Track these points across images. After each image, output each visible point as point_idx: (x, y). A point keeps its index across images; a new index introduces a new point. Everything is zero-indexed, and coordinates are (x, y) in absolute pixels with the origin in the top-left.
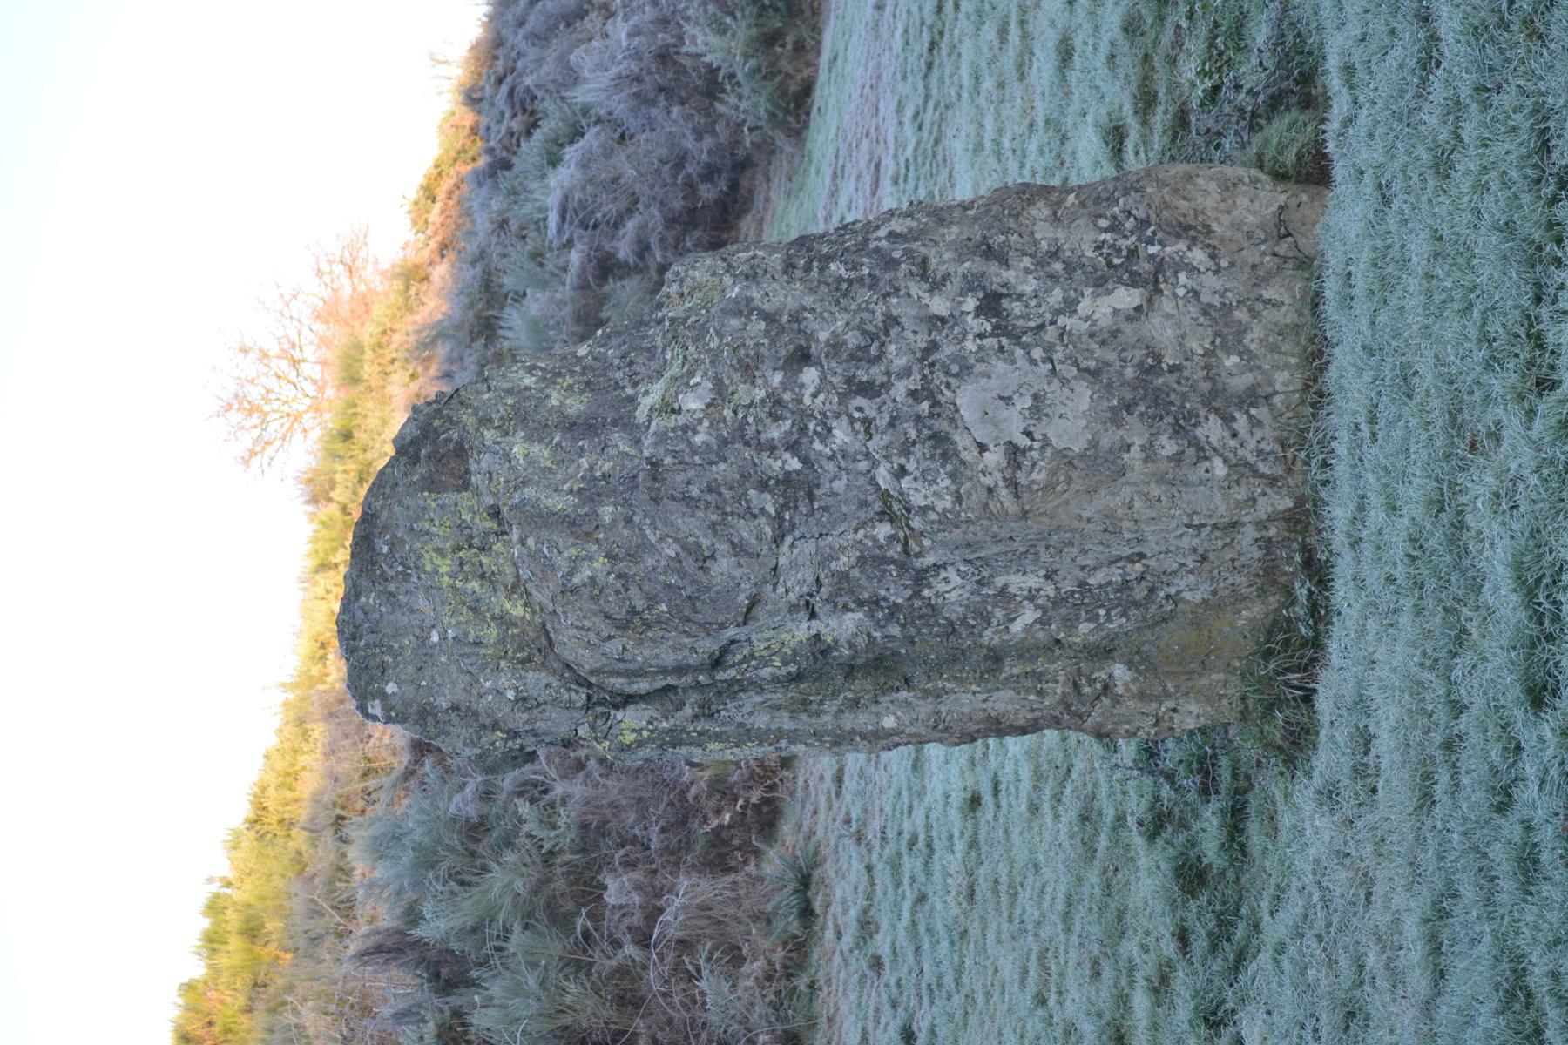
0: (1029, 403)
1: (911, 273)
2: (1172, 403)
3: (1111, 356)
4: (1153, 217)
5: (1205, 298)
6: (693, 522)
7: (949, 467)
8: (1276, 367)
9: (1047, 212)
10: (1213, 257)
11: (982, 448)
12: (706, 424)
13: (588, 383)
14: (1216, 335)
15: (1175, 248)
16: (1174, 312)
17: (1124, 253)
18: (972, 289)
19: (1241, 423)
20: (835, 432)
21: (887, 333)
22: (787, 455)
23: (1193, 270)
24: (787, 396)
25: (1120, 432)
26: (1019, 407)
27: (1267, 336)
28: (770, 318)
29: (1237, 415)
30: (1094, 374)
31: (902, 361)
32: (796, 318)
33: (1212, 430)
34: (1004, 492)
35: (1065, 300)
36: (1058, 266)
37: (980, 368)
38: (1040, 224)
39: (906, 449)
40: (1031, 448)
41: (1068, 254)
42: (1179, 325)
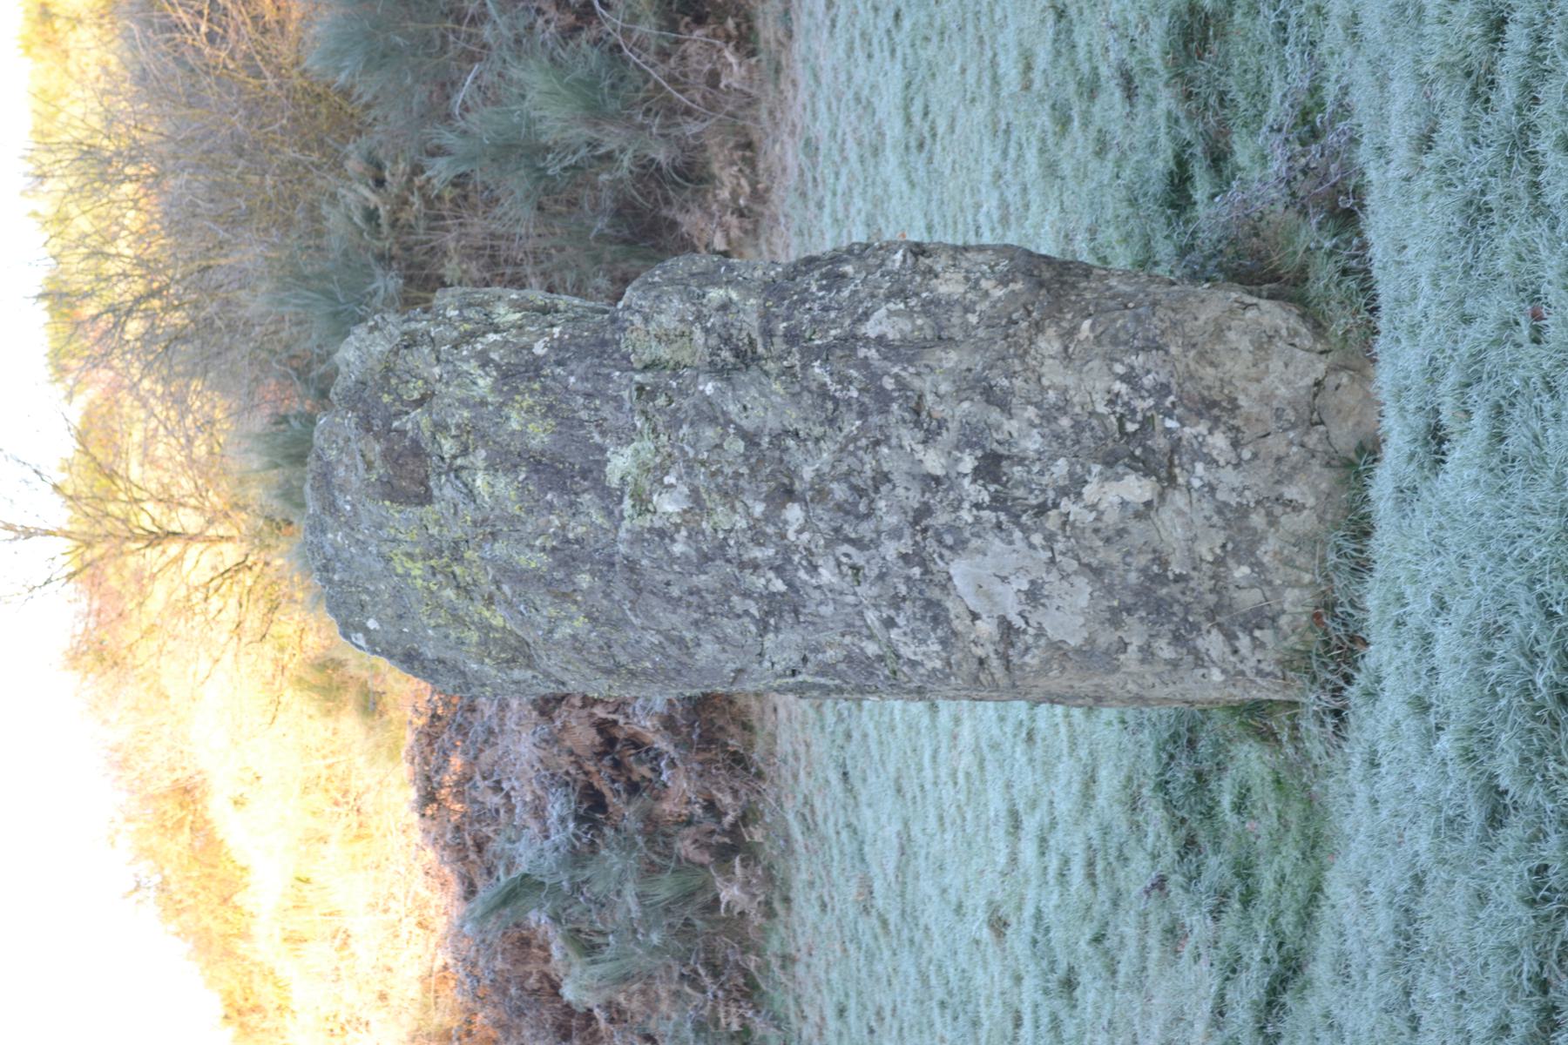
0: (1025, 587)
1: (904, 421)
2: (1174, 614)
3: (1115, 558)
4: (1174, 387)
5: (1221, 496)
6: (675, 619)
7: (940, 633)
8: (1289, 584)
9: (1057, 346)
10: (1236, 444)
11: (975, 616)
12: (684, 533)
13: (550, 407)
14: (1229, 538)
15: (1194, 431)
16: (1187, 509)
17: (1139, 417)
18: (971, 445)
19: (1244, 642)
20: (821, 570)
21: (877, 490)
22: (771, 574)
23: (1211, 462)
24: (770, 530)
25: (1119, 633)
26: (1015, 587)
27: (1282, 549)
28: (751, 439)
29: (1240, 635)
30: (1096, 572)
31: (892, 520)
32: (778, 438)
33: (1212, 643)
34: (995, 662)
35: (1071, 474)
36: (1065, 422)
37: (975, 543)
38: (1049, 362)
39: (897, 602)
40: (1025, 632)
41: (1078, 409)
42: (1189, 524)
